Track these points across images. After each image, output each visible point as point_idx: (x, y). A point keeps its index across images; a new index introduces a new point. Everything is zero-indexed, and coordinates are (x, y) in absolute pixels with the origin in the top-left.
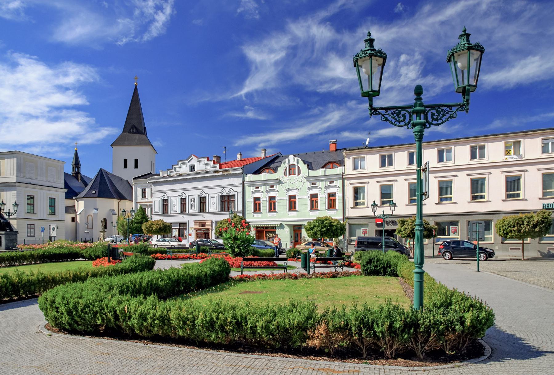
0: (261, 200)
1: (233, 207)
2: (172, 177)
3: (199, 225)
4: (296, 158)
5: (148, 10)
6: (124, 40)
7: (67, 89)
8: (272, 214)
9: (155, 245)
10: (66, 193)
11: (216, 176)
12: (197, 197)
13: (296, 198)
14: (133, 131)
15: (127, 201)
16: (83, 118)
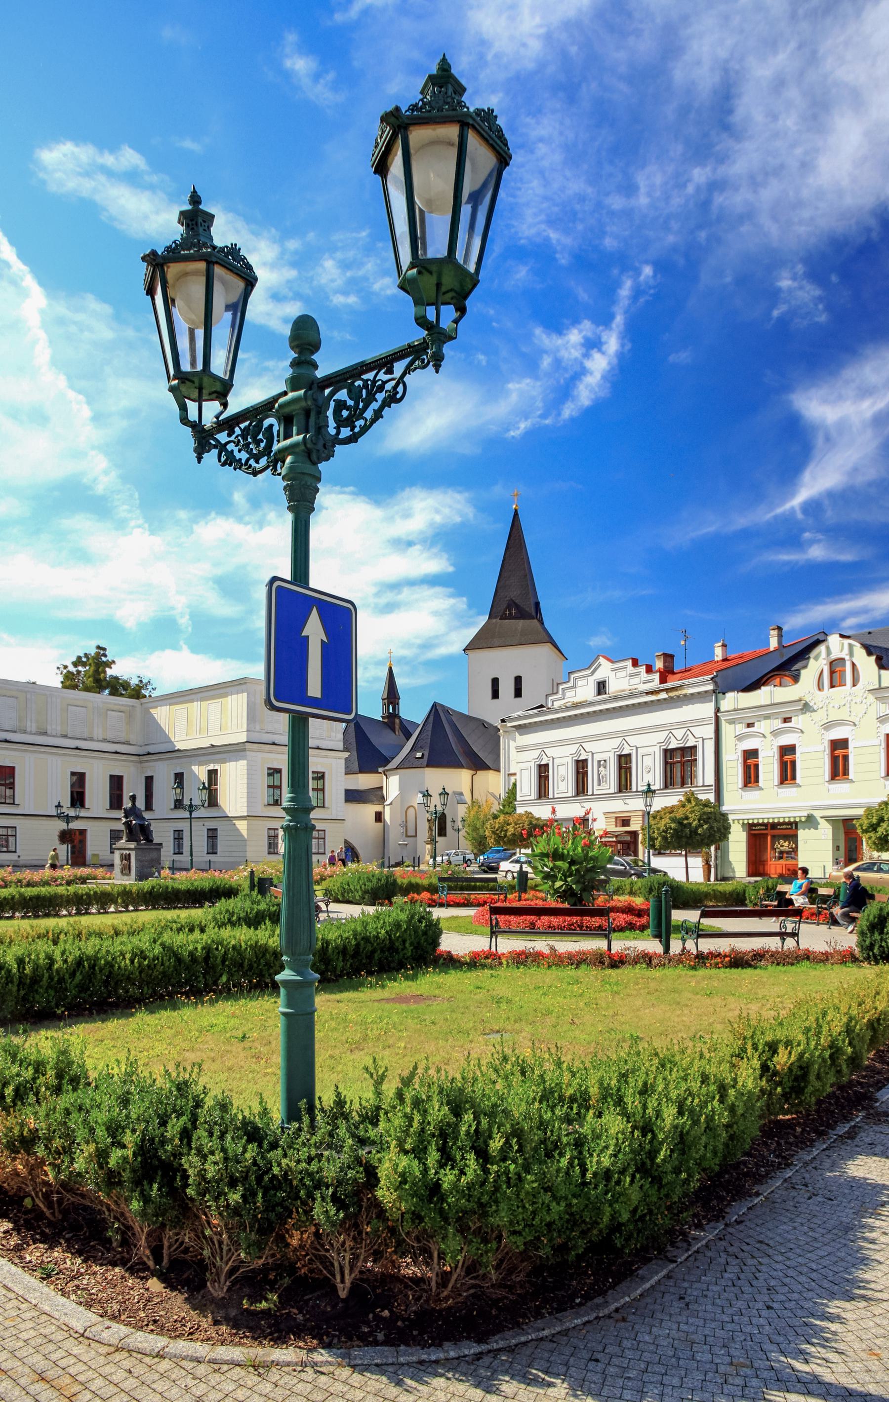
0: (761, 754)
1: (693, 776)
2: (557, 711)
3: (616, 822)
4: (847, 642)
5: (570, 353)
6: (523, 426)
7: (410, 544)
8: (788, 792)
9: (507, 872)
10: (346, 759)
11: (652, 701)
12: (611, 755)
13: (847, 748)
14: (510, 614)
15: (491, 772)
16: (441, 600)
